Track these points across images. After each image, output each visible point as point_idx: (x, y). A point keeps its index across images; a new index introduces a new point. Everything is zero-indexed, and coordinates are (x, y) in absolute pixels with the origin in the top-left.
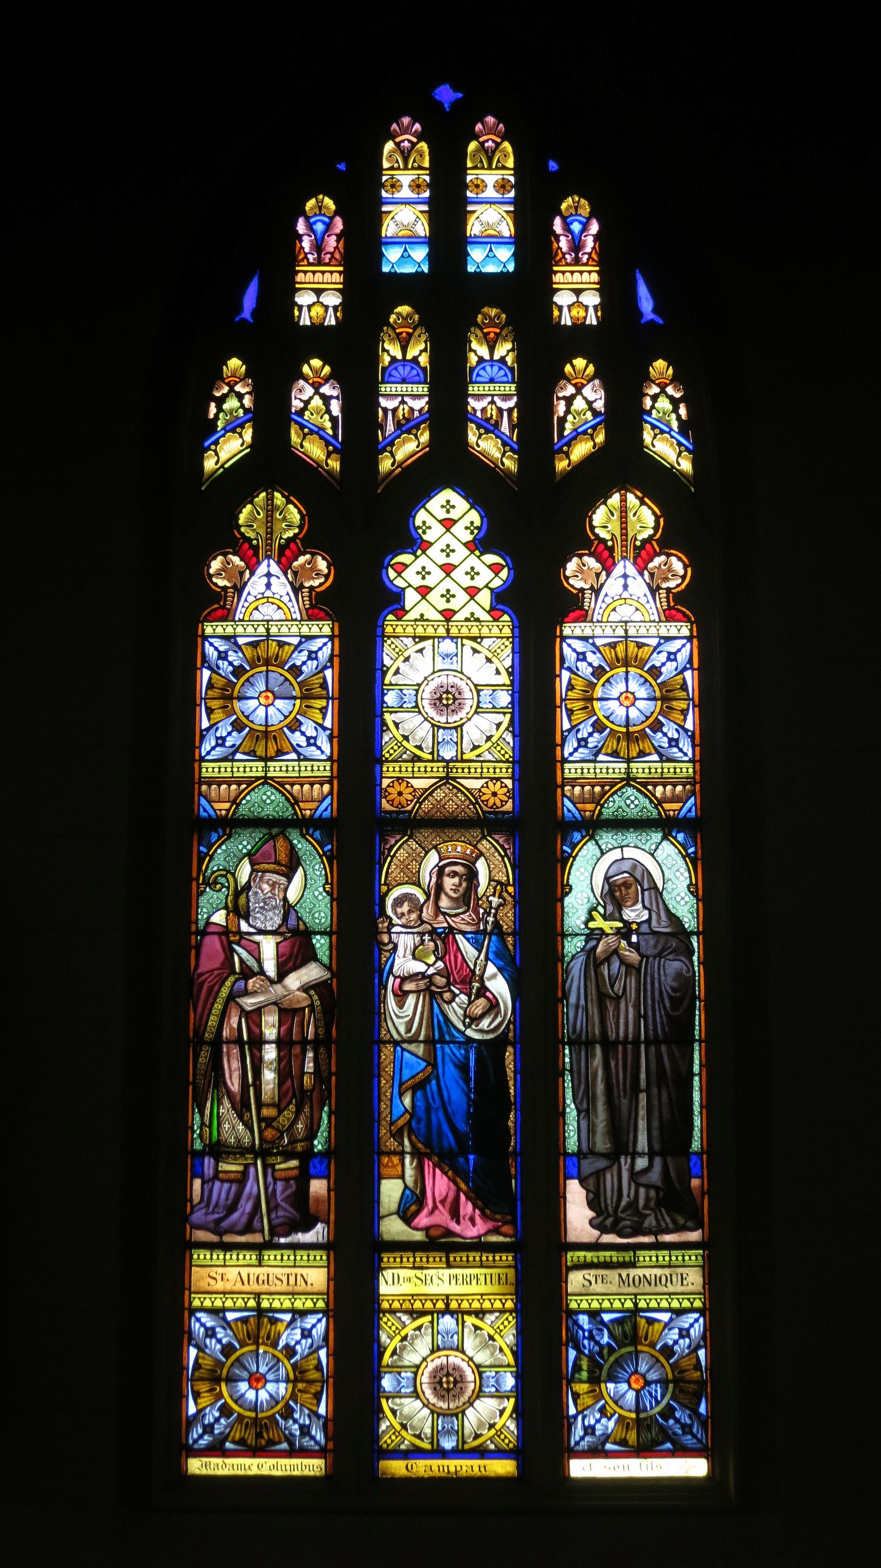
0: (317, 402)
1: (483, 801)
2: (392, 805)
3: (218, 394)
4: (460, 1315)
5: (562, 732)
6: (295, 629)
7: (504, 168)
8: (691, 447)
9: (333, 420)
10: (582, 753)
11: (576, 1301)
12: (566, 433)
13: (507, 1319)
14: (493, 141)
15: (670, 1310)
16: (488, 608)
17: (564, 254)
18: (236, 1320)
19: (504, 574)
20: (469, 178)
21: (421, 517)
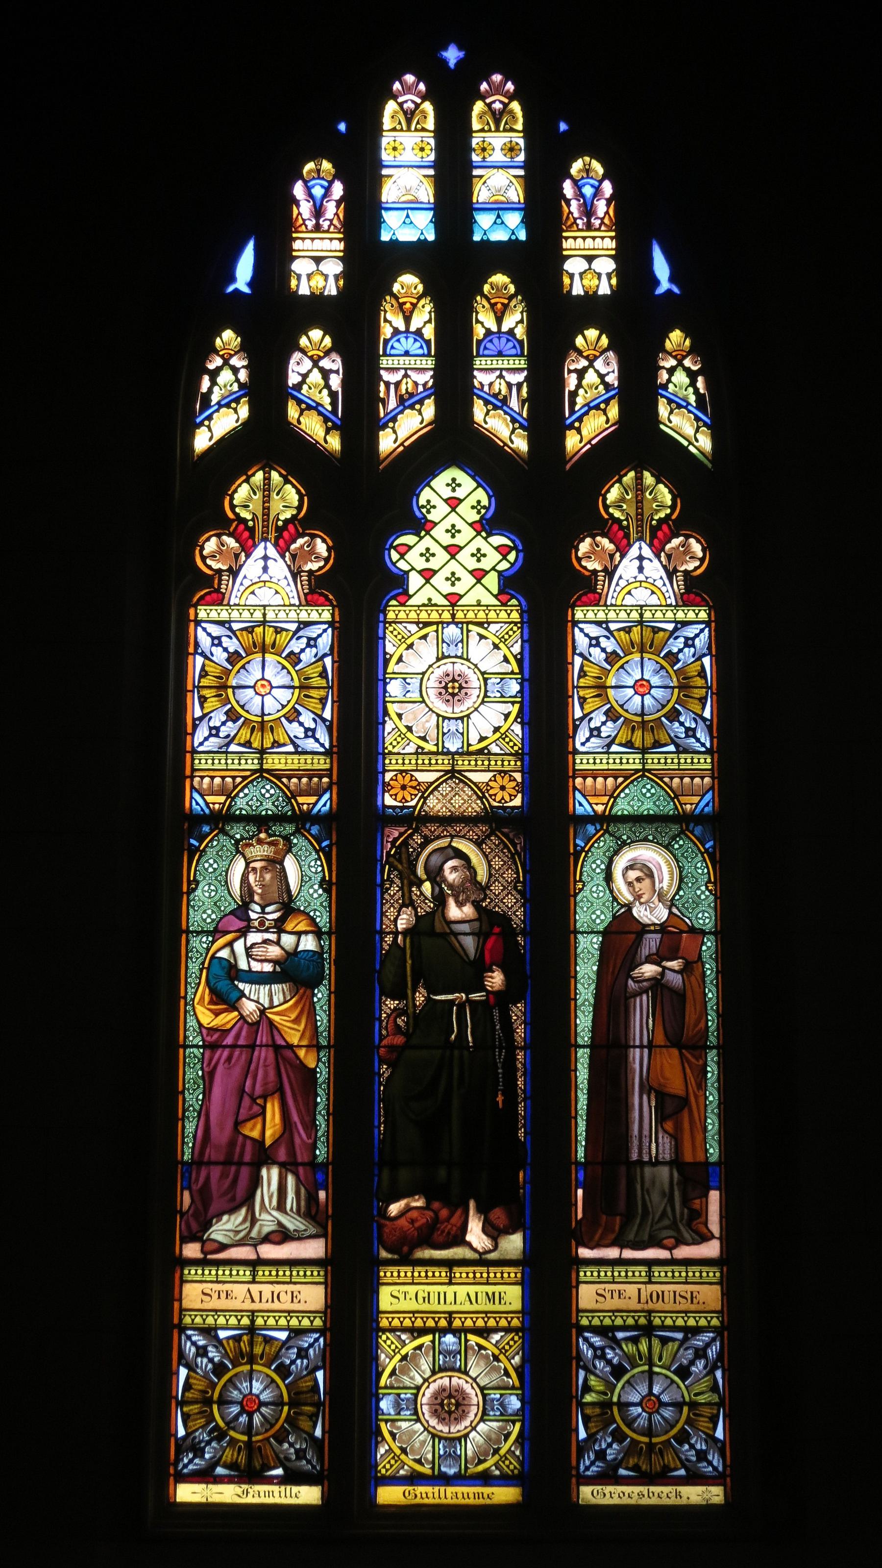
0: (316, 377)
1: (490, 796)
2: (395, 799)
3: (211, 366)
5: (194, 720)
6: (669, 615)
7: (512, 130)
8: (708, 421)
9: (333, 395)
10: (213, 743)
12: (577, 408)
15: (288, 1328)
16: (495, 592)
18: (228, 1338)
19: (512, 557)
20: (474, 142)
21: (426, 495)
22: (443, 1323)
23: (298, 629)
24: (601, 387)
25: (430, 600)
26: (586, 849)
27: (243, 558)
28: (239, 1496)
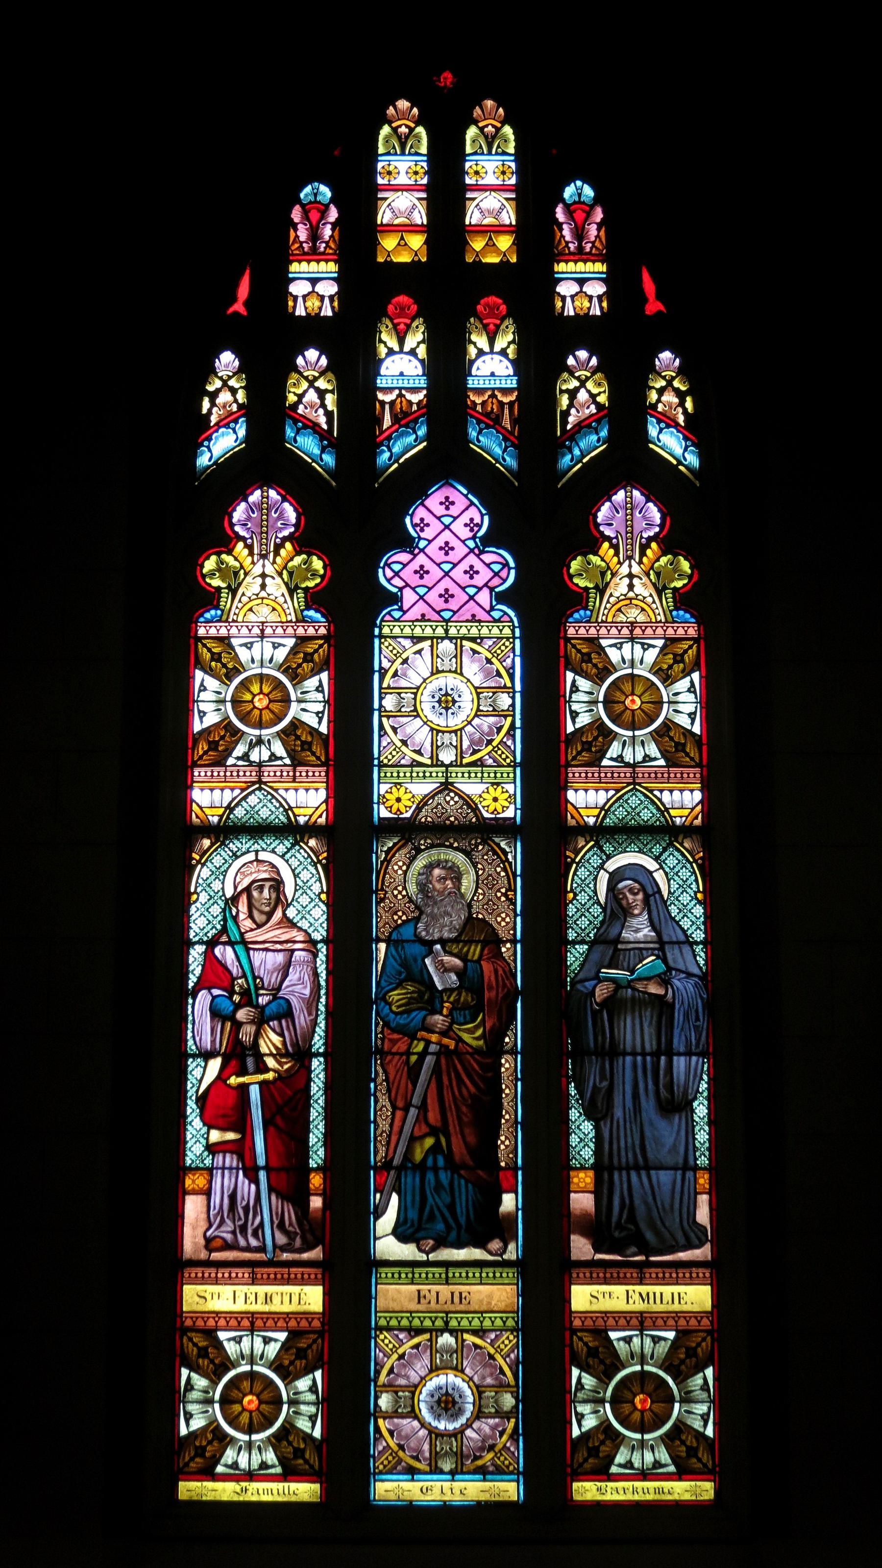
0: (312, 396)
1: (484, 807)
2: (390, 812)
3: (210, 388)
4: (459, 1334)
9: (329, 414)
11: (456, 1318)
12: (569, 427)
13: (508, 1338)
14: (493, 126)
17: (567, 243)
22: (439, 1323)
23: (296, 645)
24: (593, 407)
25: (473, 616)
26: (577, 860)
27: (609, 576)
28: (238, 1493)
